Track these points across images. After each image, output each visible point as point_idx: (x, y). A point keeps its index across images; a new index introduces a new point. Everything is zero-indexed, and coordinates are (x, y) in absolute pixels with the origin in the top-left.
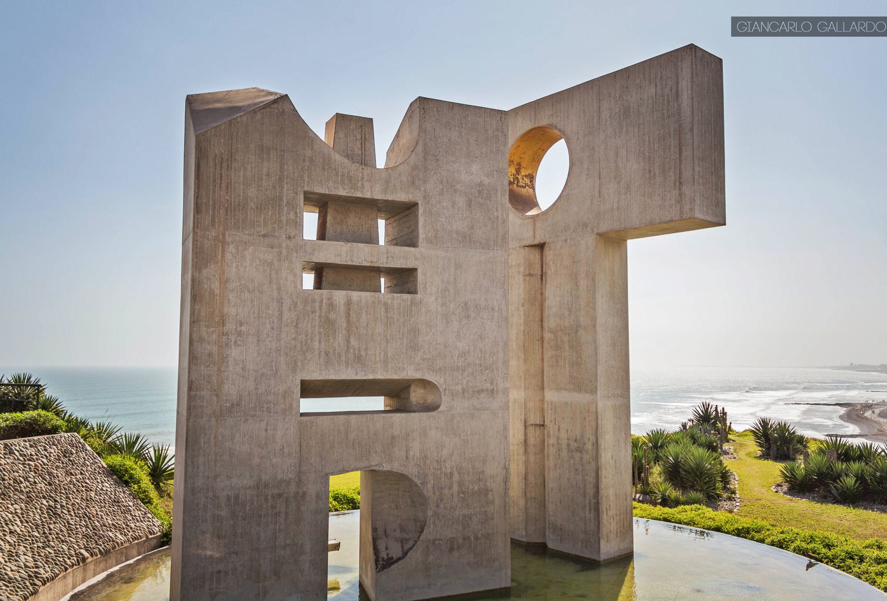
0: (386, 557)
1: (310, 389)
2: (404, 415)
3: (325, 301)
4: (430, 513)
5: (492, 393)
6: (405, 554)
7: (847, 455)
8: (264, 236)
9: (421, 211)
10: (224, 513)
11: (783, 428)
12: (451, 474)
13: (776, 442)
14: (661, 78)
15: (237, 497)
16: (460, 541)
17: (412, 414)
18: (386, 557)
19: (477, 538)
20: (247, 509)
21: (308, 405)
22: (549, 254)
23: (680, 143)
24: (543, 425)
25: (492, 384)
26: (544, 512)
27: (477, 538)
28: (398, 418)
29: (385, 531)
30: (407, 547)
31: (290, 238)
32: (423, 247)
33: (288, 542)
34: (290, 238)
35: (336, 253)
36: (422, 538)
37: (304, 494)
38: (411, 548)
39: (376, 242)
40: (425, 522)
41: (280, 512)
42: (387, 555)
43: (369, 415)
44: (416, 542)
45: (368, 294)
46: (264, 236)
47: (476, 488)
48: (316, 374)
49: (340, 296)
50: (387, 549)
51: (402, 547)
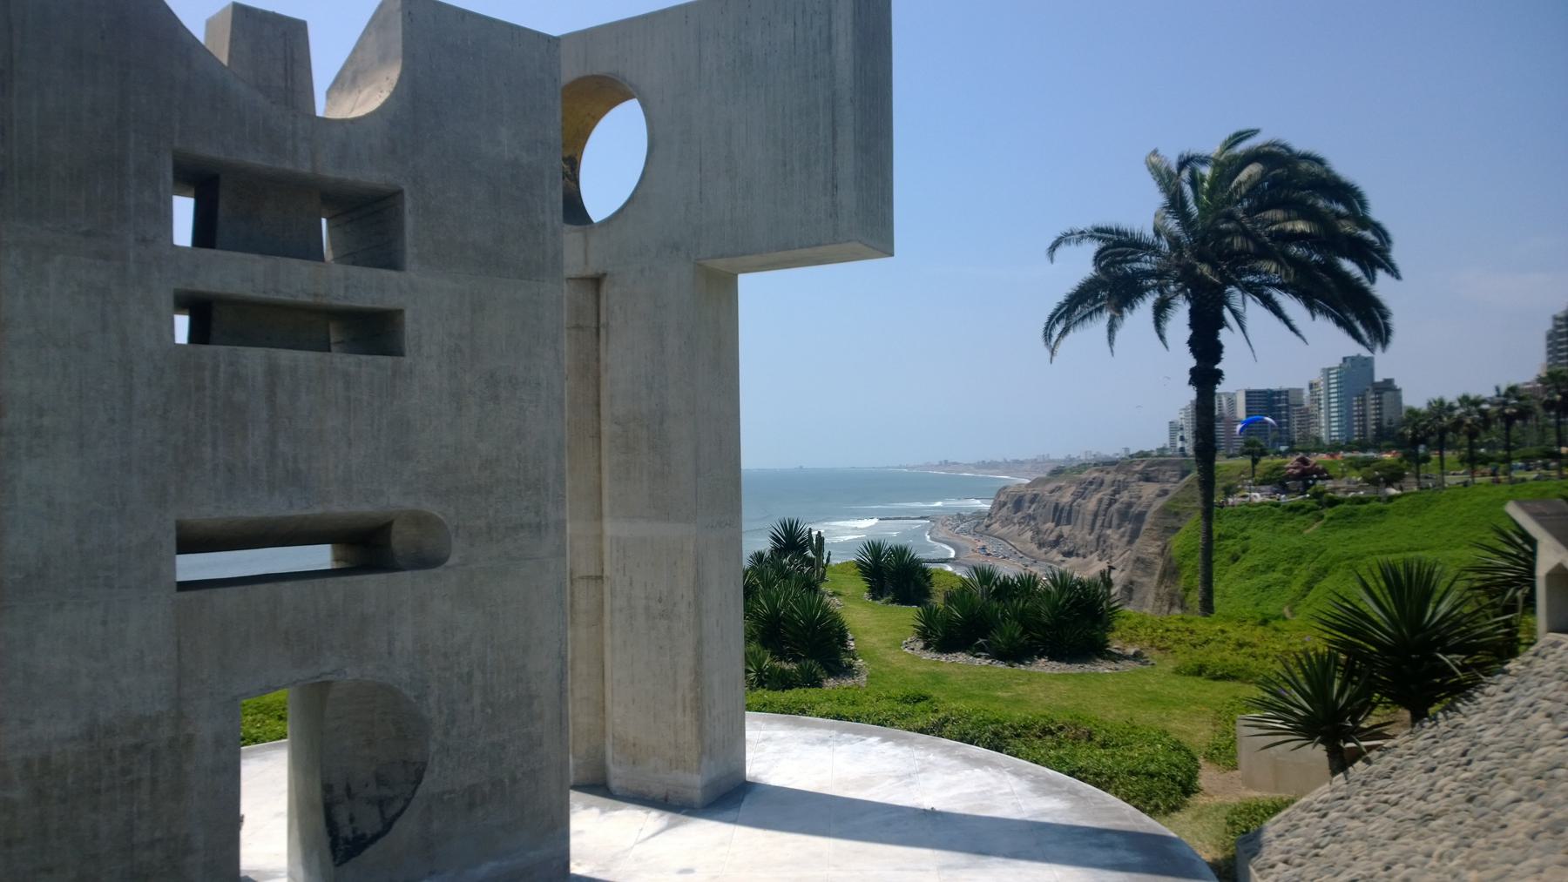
0: (351, 836)
1: (191, 542)
2: (383, 577)
3: (222, 367)
4: (433, 747)
5: (538, 529)
6: (388, 826)
7: (1005, 590)
8: (87, 234)
9: (408, 205)
10: (18, 794)
11: (900, 552)
12: (470, 675)
13: (893, 575)
14: (804, 12)
15: (45, 760)
16: (487, 789)
17: (400, 574)
18: (351, 836)
19: (514, 781)
20: (70, 780)
21: (193, 566)
22: (610, 292)
23: (834, 122)
24: (600, 578)
25: (537, 513)
26: (604, 719)
27: (514, 781)
28: (372, 583)
29: (348, 789)
30: (391, 812)
31: (144, 240)
32: (413, 272)
33: (158, 834)
34: (144, 240)
35: (238, 275)
36: (419, 792)
37: (190, 739)
38: (399, 814)
39: (321, 258)
40: (425, 764)
41: (140, 780)
42: (354, 831)
43: (316, 581)
44: (408, 801)
45: (312, 355)
46: (87, 234)
47: (512, 695)
48: (208, 512)
49: (254, 358)
50: (352, 820)
51: (382, 813)
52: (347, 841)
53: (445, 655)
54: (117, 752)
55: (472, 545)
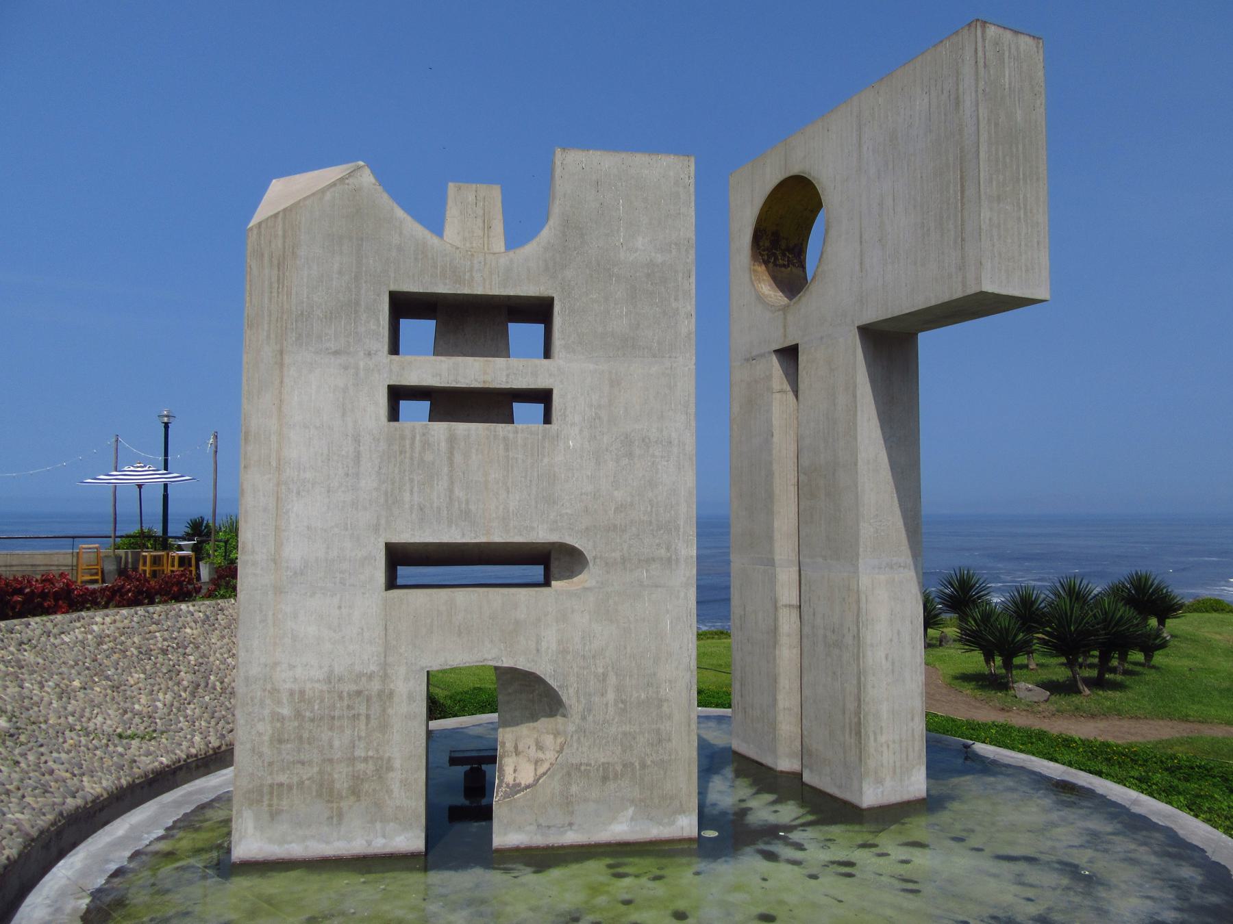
0: (511, 782)
3: (418, 438)
12: (605, 675)
16: (619, 768)
18: (511, 782)
19: (643, 766)
25: (668, 549)
27: (643, 766)
31: (369, 354)
33: (370, 753)
46: (336, 353)
52: (508, 785)
53: (584, 657)
54: (345, 694)
55: (608, 572)
